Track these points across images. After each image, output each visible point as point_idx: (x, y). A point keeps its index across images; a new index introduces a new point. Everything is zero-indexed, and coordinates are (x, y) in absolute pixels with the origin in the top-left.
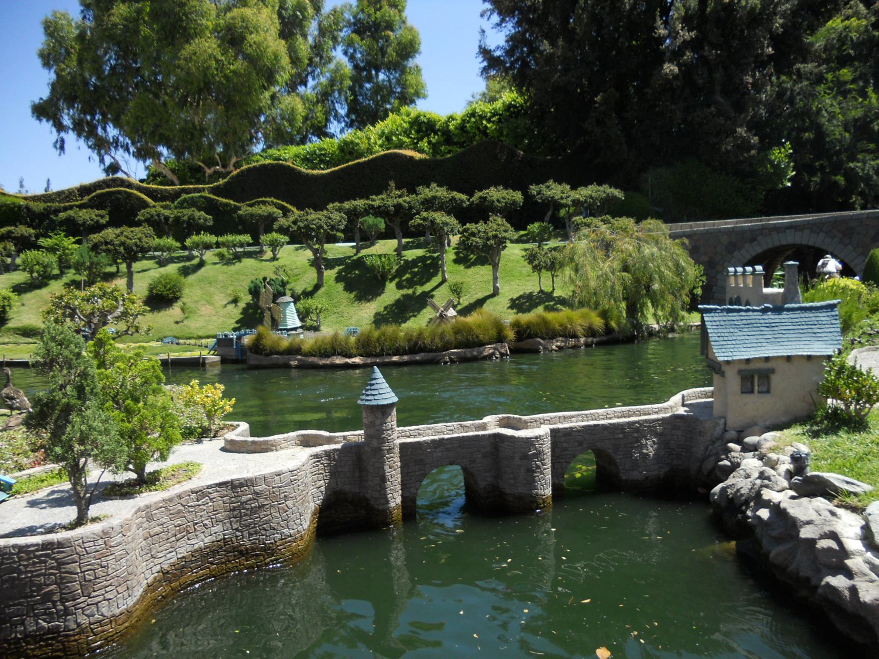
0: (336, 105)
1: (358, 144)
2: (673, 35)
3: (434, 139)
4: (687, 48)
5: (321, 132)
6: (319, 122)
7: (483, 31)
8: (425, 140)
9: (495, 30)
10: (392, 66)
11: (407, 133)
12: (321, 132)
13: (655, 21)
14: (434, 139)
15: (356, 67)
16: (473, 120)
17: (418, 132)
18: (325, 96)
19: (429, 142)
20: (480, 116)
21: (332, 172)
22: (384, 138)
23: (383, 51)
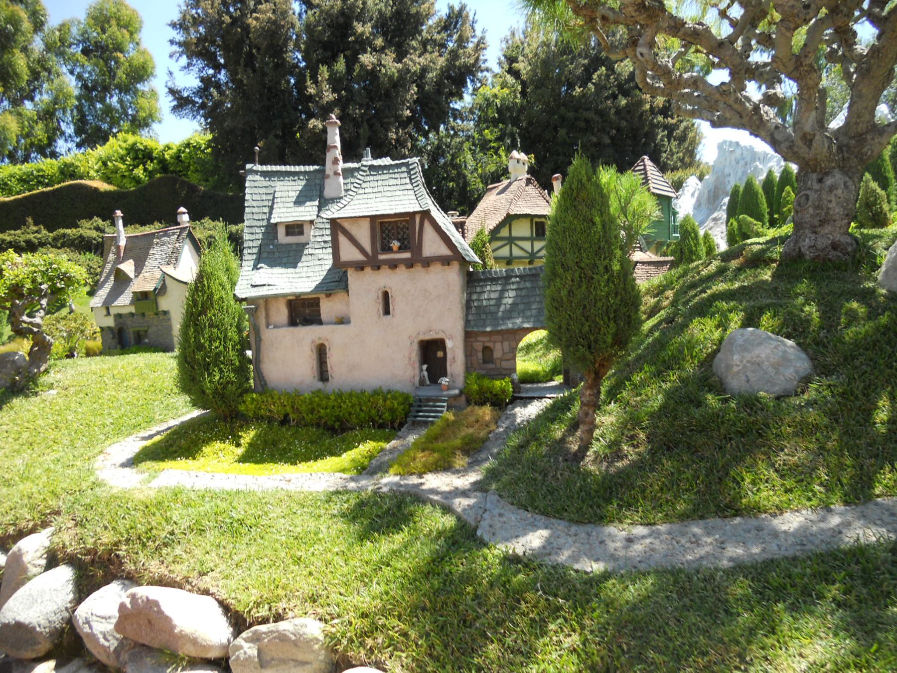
0: (62, 123)
1: (77, 167)
2: (320, 94)
3: (150, 166)
4: (336, 106)
5: (46, 149)
6: (40, 140)
7: (171, 73)
8: (141, 167)
9: (182, 73)
10: (125, 89)
11: (122, 159)
12: (46, 149)
13: (306, 82)
14: (150, 166)
15: (85, 86)
16: (187, 150)
17: (134, 159)
18: (47, 115)
19: (145, 170)
20: (194, 147)
21: (15, 200)
22: (100, 163)
23: (112, 74)
